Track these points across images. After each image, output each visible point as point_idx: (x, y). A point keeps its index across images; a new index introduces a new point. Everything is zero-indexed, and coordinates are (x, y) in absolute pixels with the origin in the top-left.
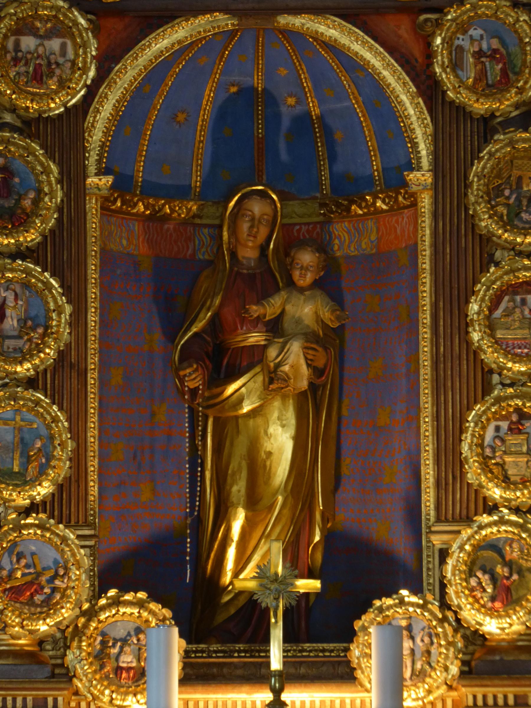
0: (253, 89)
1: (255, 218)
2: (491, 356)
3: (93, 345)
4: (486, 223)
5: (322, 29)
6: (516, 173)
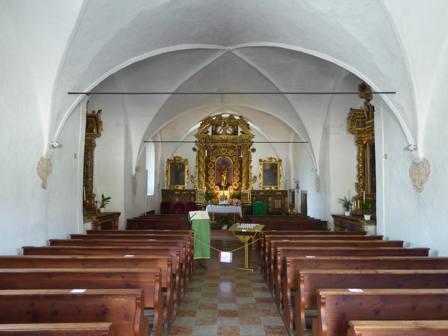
1: (224, 166)
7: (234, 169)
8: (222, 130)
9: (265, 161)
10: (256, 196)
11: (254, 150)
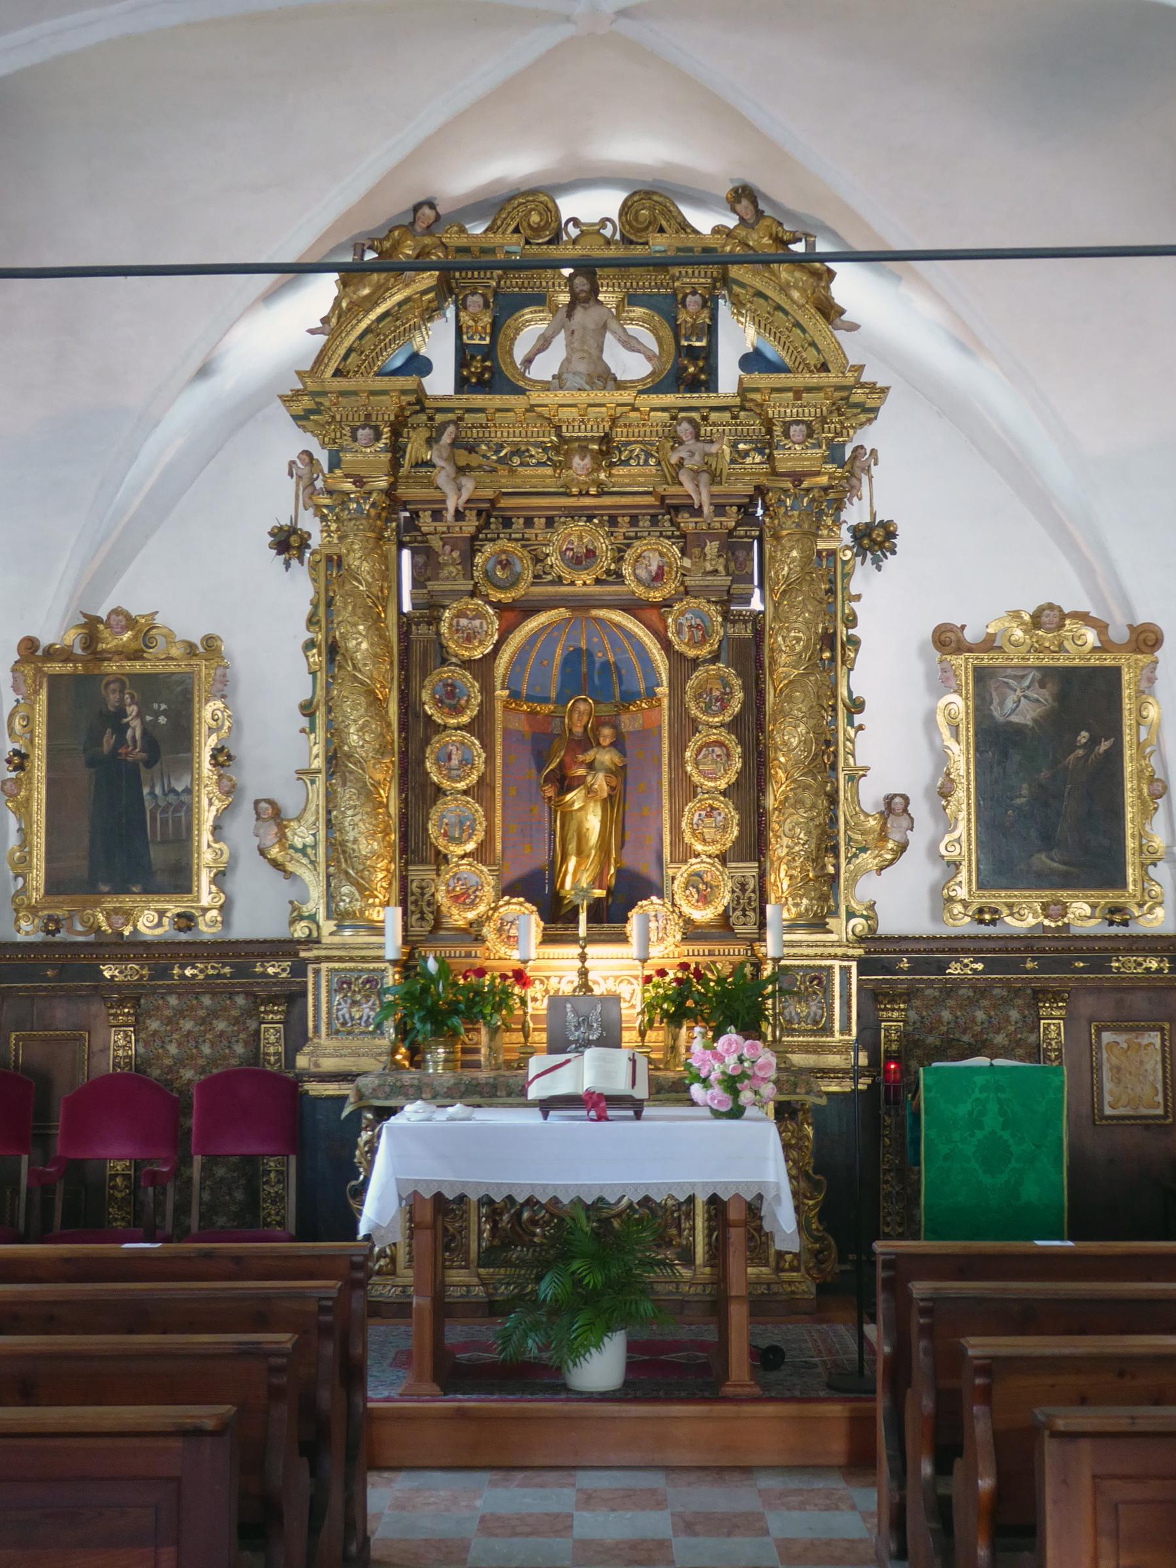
0: (580, 649)
1: (581, 712)
2: (697, 779)
3: (499, 774)
4: (694, 712)
5: (613, 617)
6: (709, 686)
7: (684, 727)
8: (560, 340)
9: (989, 644)
10: (908, 996)
11: (876, 540)
